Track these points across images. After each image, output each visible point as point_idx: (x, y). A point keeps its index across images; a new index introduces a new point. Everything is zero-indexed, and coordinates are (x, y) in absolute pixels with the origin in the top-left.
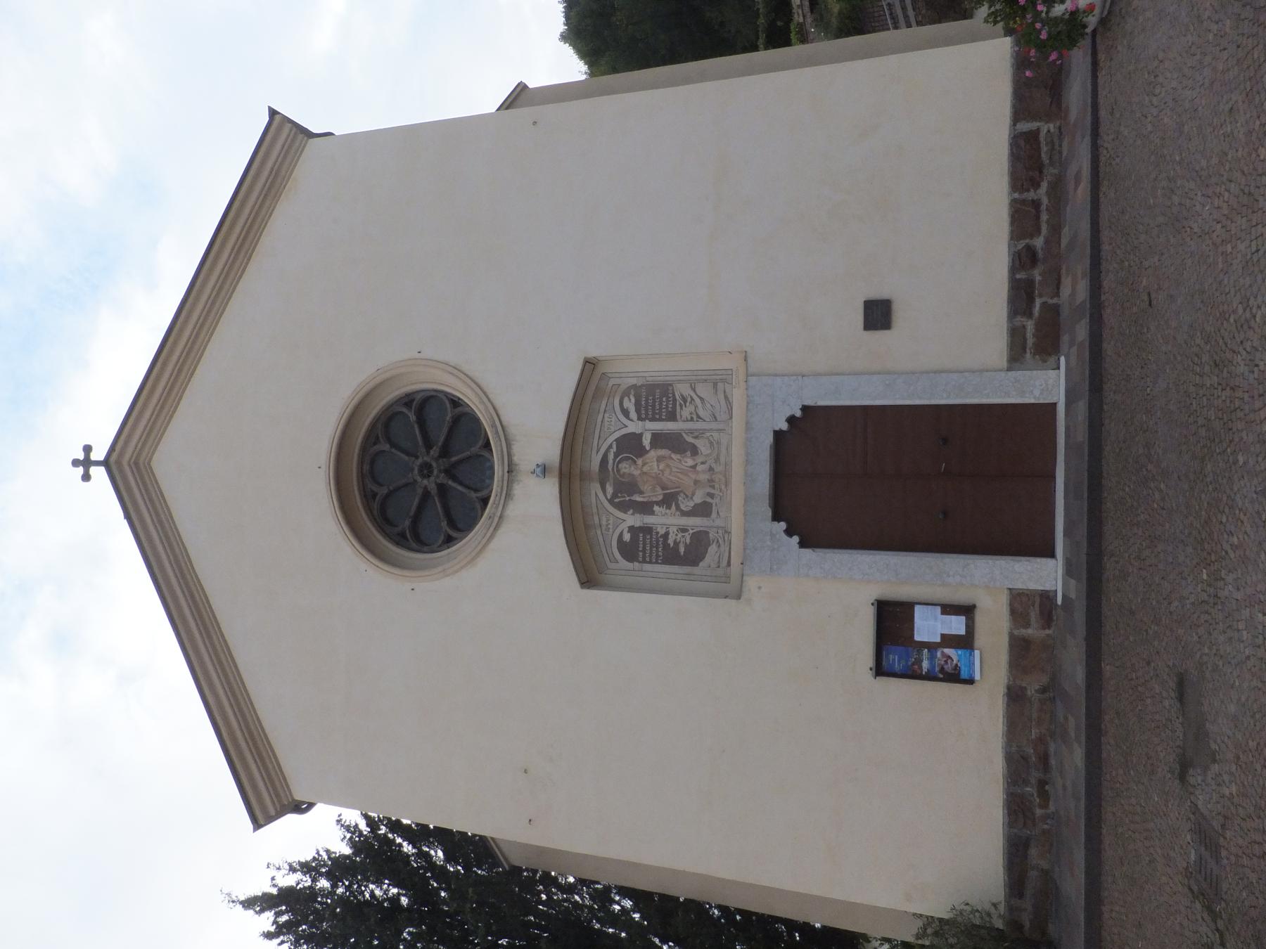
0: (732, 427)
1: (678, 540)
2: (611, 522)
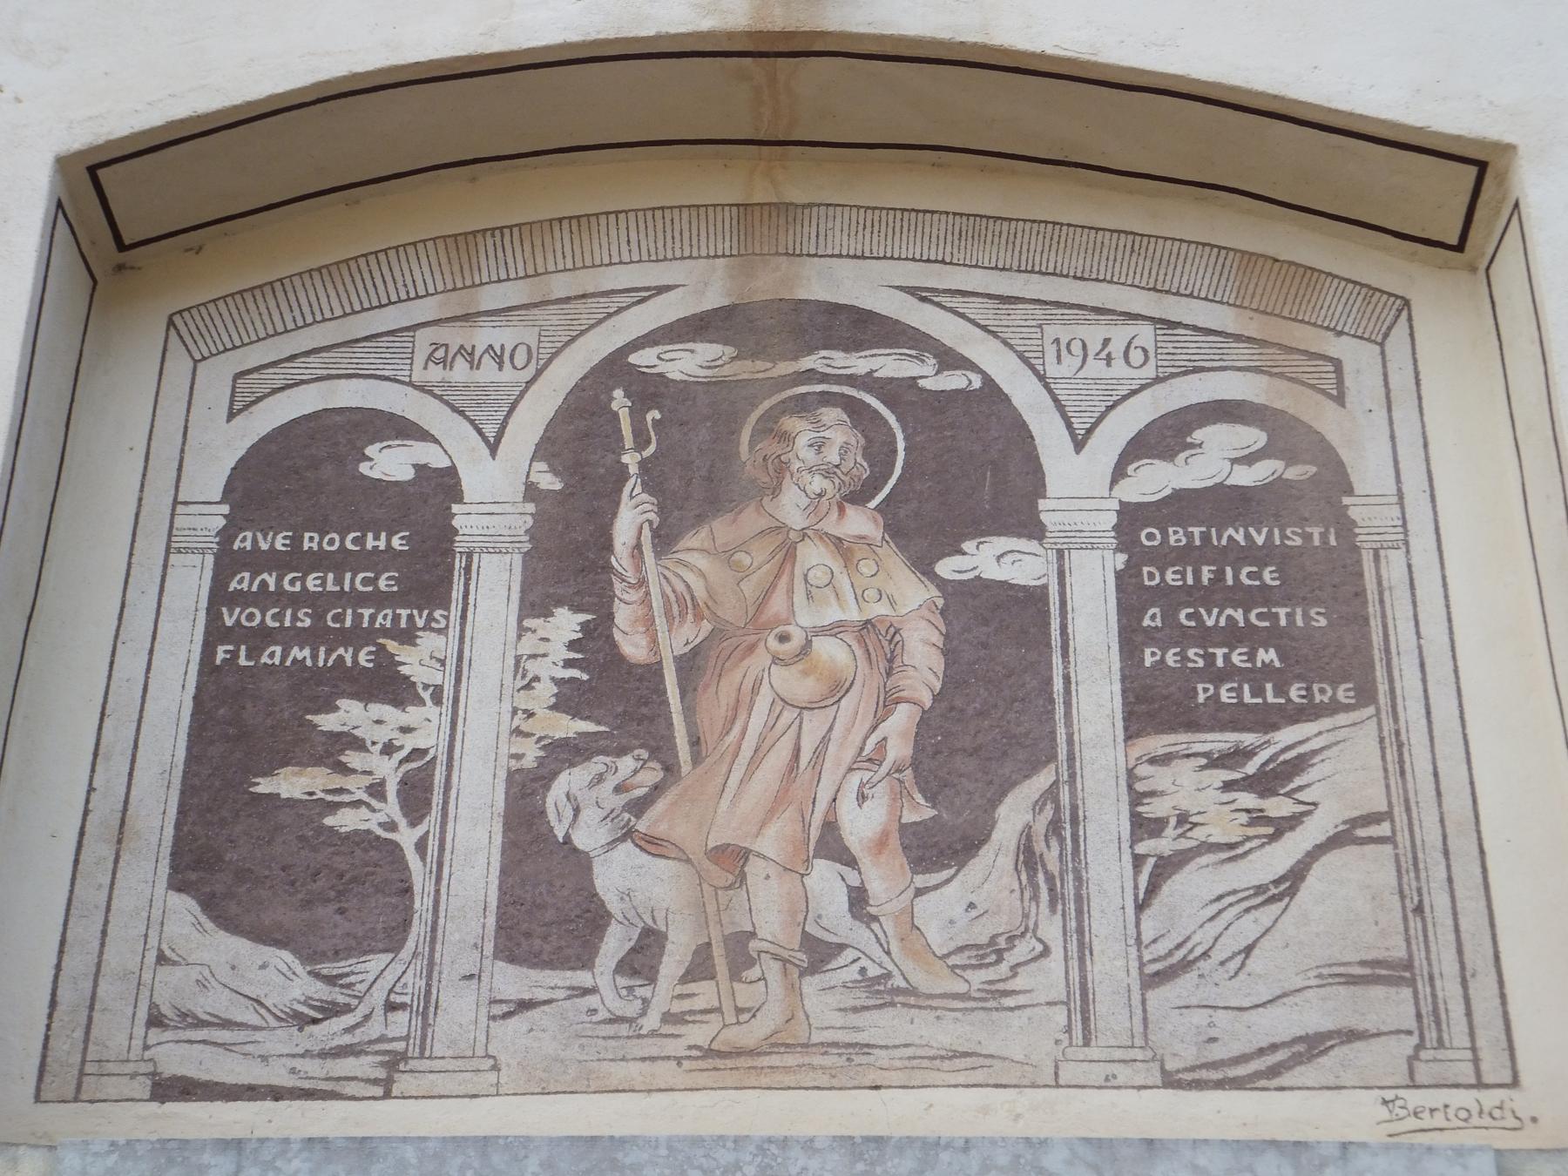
0: (1109, 1083)
1: (352, 759)
2: (488, 372)
